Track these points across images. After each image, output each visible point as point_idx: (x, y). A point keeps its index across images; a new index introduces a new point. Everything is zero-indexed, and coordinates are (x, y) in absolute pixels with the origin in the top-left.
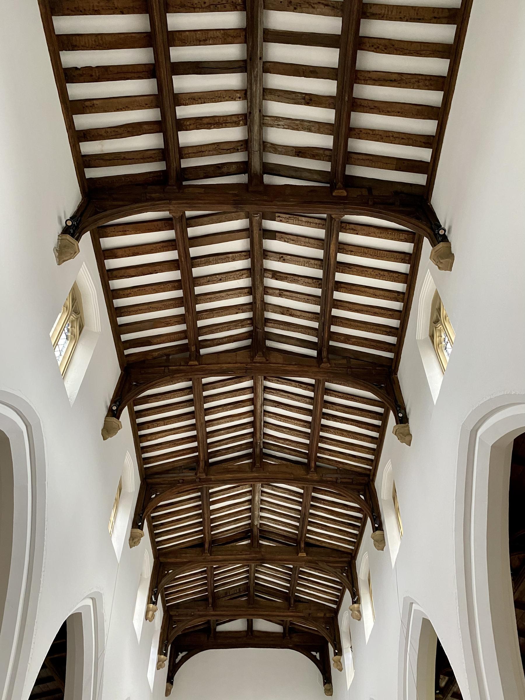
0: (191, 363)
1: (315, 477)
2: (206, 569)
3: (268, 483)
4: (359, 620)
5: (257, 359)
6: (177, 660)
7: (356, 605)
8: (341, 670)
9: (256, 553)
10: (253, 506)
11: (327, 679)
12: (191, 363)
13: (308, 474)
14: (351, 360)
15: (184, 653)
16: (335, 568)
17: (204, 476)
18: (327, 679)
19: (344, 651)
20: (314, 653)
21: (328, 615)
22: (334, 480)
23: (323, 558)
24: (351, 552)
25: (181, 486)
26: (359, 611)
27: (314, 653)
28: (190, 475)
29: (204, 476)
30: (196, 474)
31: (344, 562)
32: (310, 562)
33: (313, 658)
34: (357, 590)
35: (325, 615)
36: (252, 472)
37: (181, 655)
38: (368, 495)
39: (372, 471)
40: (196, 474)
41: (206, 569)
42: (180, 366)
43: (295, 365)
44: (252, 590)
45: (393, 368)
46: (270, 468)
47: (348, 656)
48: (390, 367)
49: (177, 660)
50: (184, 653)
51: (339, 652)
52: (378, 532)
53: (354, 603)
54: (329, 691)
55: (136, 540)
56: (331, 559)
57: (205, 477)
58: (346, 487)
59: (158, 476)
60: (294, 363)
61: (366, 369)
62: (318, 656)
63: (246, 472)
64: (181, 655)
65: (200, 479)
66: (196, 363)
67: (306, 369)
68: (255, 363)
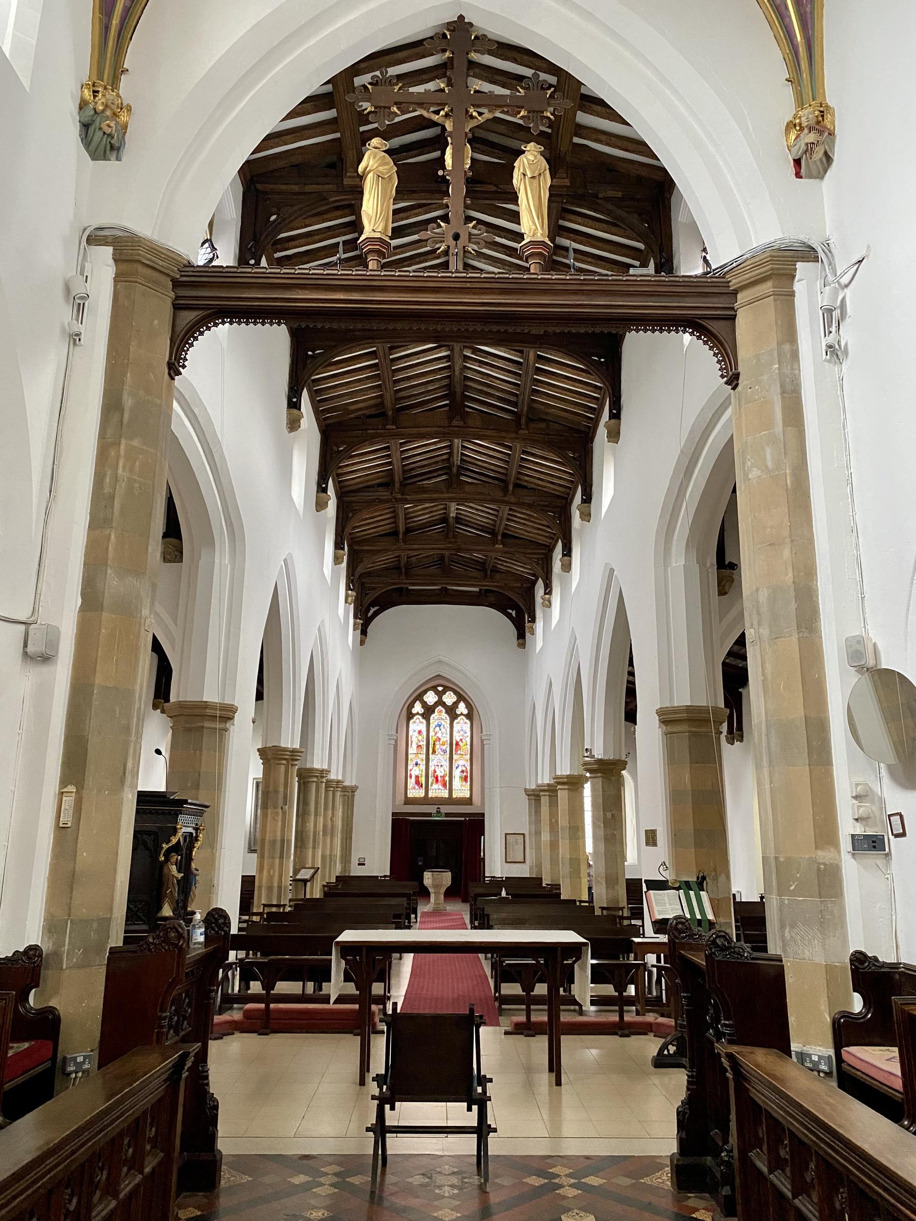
0: (388, 427)
1: (513, 499)
2: (375, 349)
3: (472, 345)
4: (550, 607)
5: (455, 423)
6: (369, 615)
7: (547, 596)
8: (533, 634)
9: (450, 543)
10: (453, 362)
11: (521, 635)
12: (388, 427)
13: (505, 496)
14: (551, 423)
15: (376, 608)
16: (530, 558)
17: (399, 496)
18: (521, 635)
19: (537, 620)
20: (510, 611)
21: (524, 585)
22: (531, 502)
23: (520, 550)
24: (587, 430)
25: (377, 505)
26: (550, 601)
27: (510, 611)
28: (384, 494)
29: (399, 496)
30: (391, 494)
31: (542, 553)
32: (506, 553)
33: (509, 616)
34: (551, 582)
35: (522, 585)
36: (448, 492)
37: (372, 610)
38: (563, 518)
39: (592, 429)
40: (391, 494)
41: (375, 349)
42: (378, 429)
43: (493, 429)
44: (446, 560)
45: (590, 435)
46: (468, 488)
47: (539, 625)
48: (567, 499)
49: (369, 615)
50: (376, 608)
51: (533, 620)
52: (566, 558)
53: (545, 594)
54: (522, 645)
55: (340, 560)
56: (529, 551)
57: (400, 497)
58: (542, 510)
59: (354, 494)
60: (492, 427)
61: (563, 436)
62: (514, 613)
63: (442, 492)
64: (372, 610)
65: (396, 498)
66: (394, 427)
67: (503, 434)
68: (452, 427)
